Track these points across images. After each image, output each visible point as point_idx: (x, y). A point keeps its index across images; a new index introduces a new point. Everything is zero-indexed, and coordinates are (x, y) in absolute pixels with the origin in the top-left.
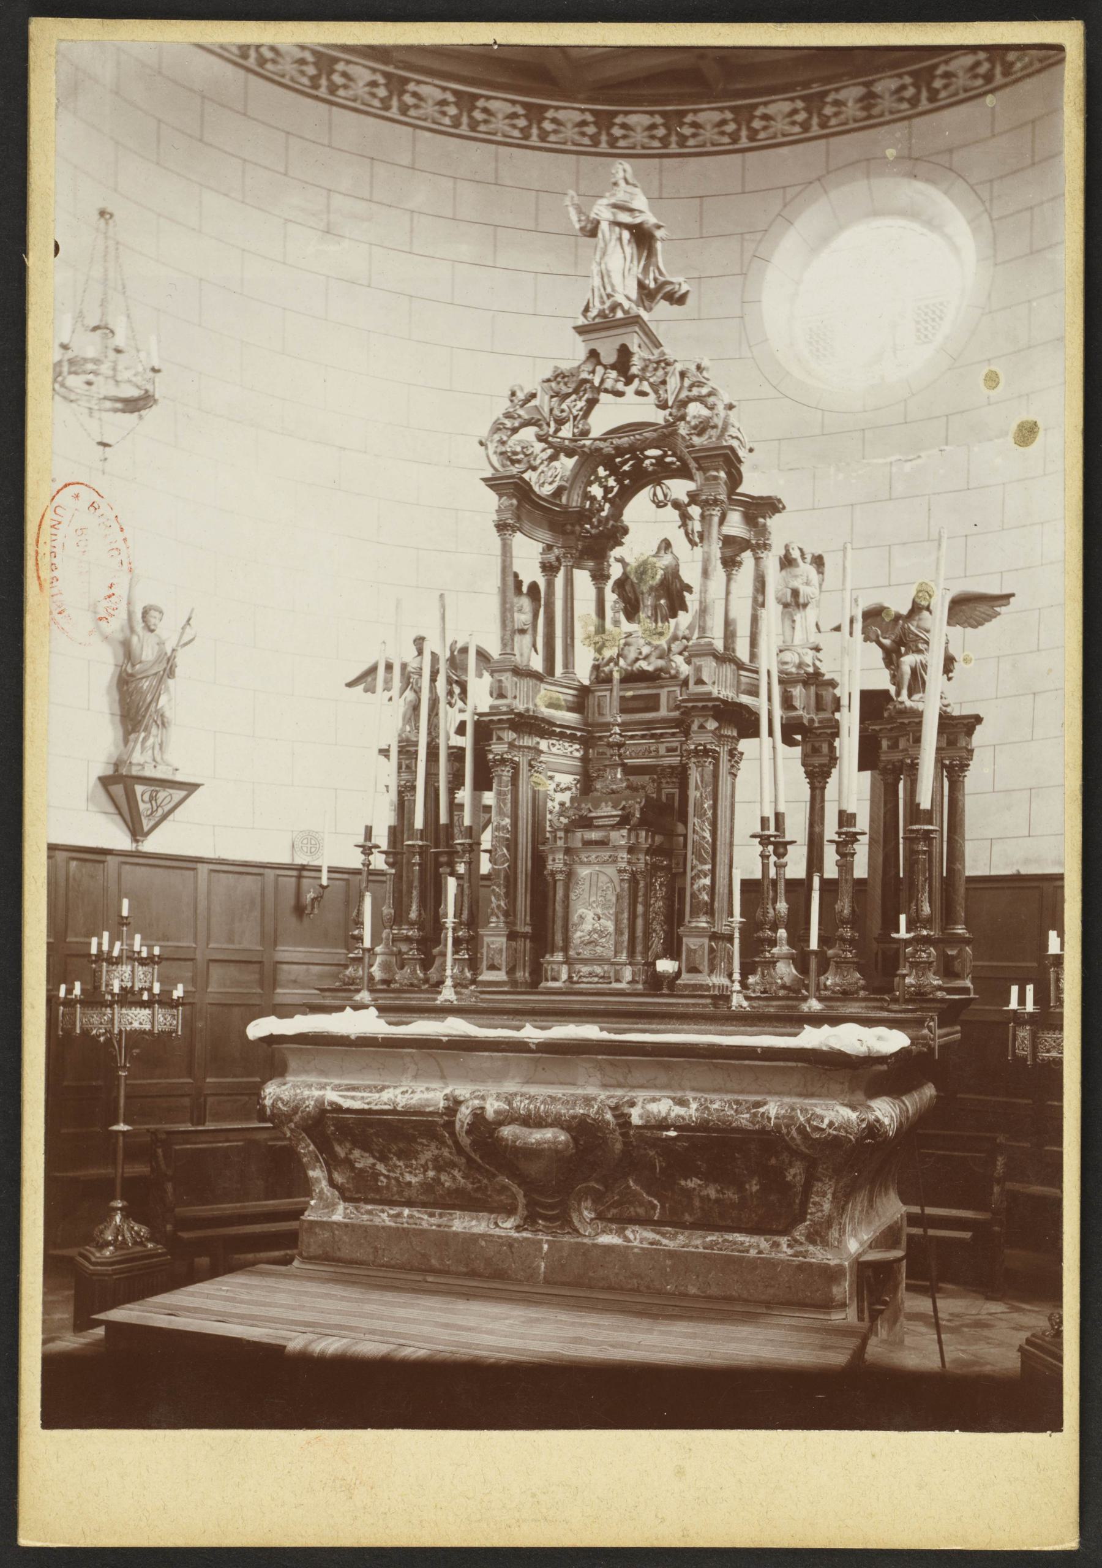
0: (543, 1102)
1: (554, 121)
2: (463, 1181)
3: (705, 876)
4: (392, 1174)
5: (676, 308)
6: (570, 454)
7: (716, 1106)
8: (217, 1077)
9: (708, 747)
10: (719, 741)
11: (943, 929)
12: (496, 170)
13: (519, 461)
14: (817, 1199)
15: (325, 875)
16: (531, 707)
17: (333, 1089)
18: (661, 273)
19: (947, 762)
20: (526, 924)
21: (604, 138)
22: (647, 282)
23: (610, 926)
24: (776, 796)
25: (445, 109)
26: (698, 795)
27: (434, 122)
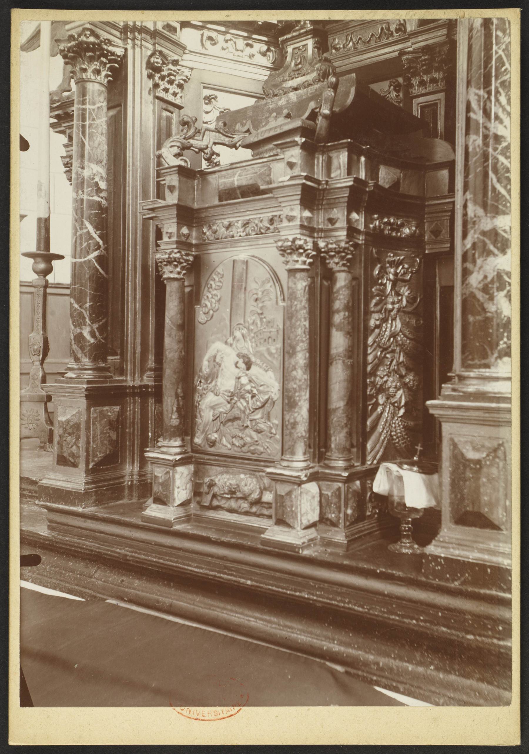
23: (270, 382)
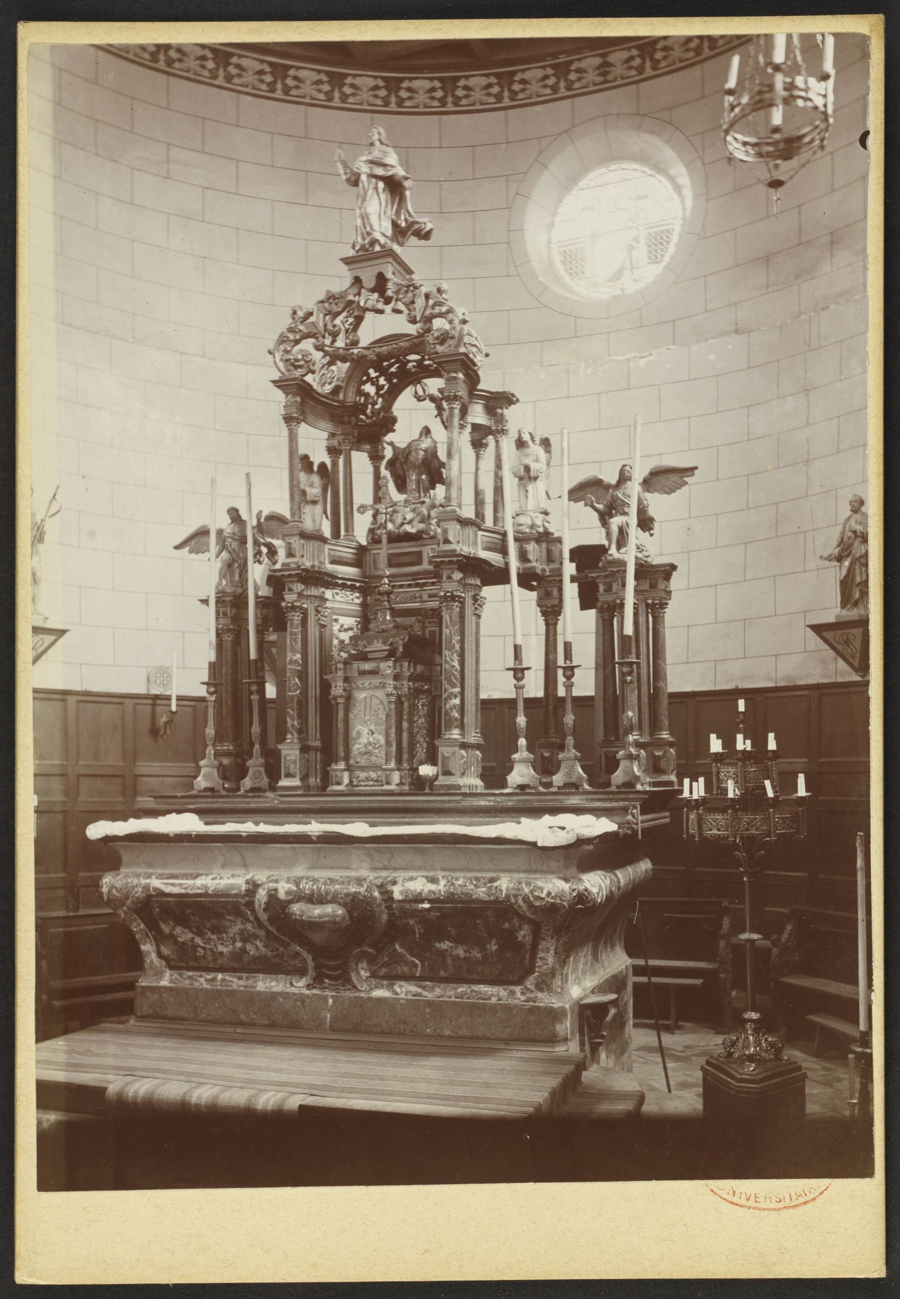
0: (325, 883)
1: (352, 86)
2: (264, 949)
3: (456, 697)
4: (207, 946)
5: (423, 242)
6: (344, 360)
7: (460, 882)
8: (88, 871)
9: (455, 593)
10: (464, 588)
11: (651, 735)
12: (306, 126)
13: (301, 367)
14: (543, 955)
15: (174, 703)
16: (317, 563)
17: (157, 878)
18: (410, 215)
19: (650, 601)
20: (316, 740)
21: (393, 99)
22: (399, 222)
23: (382, 739)
24: (514, 632)
25: (263, 77)
26: (448, 632)
27: (254, 88)
